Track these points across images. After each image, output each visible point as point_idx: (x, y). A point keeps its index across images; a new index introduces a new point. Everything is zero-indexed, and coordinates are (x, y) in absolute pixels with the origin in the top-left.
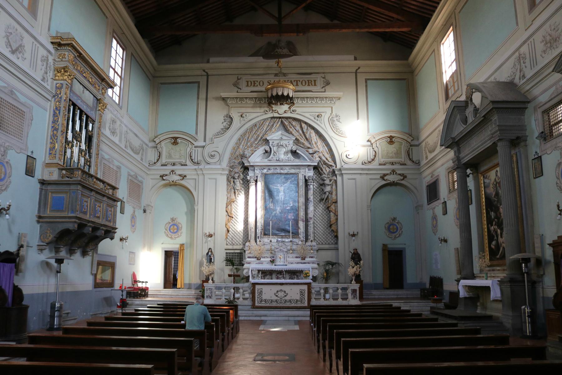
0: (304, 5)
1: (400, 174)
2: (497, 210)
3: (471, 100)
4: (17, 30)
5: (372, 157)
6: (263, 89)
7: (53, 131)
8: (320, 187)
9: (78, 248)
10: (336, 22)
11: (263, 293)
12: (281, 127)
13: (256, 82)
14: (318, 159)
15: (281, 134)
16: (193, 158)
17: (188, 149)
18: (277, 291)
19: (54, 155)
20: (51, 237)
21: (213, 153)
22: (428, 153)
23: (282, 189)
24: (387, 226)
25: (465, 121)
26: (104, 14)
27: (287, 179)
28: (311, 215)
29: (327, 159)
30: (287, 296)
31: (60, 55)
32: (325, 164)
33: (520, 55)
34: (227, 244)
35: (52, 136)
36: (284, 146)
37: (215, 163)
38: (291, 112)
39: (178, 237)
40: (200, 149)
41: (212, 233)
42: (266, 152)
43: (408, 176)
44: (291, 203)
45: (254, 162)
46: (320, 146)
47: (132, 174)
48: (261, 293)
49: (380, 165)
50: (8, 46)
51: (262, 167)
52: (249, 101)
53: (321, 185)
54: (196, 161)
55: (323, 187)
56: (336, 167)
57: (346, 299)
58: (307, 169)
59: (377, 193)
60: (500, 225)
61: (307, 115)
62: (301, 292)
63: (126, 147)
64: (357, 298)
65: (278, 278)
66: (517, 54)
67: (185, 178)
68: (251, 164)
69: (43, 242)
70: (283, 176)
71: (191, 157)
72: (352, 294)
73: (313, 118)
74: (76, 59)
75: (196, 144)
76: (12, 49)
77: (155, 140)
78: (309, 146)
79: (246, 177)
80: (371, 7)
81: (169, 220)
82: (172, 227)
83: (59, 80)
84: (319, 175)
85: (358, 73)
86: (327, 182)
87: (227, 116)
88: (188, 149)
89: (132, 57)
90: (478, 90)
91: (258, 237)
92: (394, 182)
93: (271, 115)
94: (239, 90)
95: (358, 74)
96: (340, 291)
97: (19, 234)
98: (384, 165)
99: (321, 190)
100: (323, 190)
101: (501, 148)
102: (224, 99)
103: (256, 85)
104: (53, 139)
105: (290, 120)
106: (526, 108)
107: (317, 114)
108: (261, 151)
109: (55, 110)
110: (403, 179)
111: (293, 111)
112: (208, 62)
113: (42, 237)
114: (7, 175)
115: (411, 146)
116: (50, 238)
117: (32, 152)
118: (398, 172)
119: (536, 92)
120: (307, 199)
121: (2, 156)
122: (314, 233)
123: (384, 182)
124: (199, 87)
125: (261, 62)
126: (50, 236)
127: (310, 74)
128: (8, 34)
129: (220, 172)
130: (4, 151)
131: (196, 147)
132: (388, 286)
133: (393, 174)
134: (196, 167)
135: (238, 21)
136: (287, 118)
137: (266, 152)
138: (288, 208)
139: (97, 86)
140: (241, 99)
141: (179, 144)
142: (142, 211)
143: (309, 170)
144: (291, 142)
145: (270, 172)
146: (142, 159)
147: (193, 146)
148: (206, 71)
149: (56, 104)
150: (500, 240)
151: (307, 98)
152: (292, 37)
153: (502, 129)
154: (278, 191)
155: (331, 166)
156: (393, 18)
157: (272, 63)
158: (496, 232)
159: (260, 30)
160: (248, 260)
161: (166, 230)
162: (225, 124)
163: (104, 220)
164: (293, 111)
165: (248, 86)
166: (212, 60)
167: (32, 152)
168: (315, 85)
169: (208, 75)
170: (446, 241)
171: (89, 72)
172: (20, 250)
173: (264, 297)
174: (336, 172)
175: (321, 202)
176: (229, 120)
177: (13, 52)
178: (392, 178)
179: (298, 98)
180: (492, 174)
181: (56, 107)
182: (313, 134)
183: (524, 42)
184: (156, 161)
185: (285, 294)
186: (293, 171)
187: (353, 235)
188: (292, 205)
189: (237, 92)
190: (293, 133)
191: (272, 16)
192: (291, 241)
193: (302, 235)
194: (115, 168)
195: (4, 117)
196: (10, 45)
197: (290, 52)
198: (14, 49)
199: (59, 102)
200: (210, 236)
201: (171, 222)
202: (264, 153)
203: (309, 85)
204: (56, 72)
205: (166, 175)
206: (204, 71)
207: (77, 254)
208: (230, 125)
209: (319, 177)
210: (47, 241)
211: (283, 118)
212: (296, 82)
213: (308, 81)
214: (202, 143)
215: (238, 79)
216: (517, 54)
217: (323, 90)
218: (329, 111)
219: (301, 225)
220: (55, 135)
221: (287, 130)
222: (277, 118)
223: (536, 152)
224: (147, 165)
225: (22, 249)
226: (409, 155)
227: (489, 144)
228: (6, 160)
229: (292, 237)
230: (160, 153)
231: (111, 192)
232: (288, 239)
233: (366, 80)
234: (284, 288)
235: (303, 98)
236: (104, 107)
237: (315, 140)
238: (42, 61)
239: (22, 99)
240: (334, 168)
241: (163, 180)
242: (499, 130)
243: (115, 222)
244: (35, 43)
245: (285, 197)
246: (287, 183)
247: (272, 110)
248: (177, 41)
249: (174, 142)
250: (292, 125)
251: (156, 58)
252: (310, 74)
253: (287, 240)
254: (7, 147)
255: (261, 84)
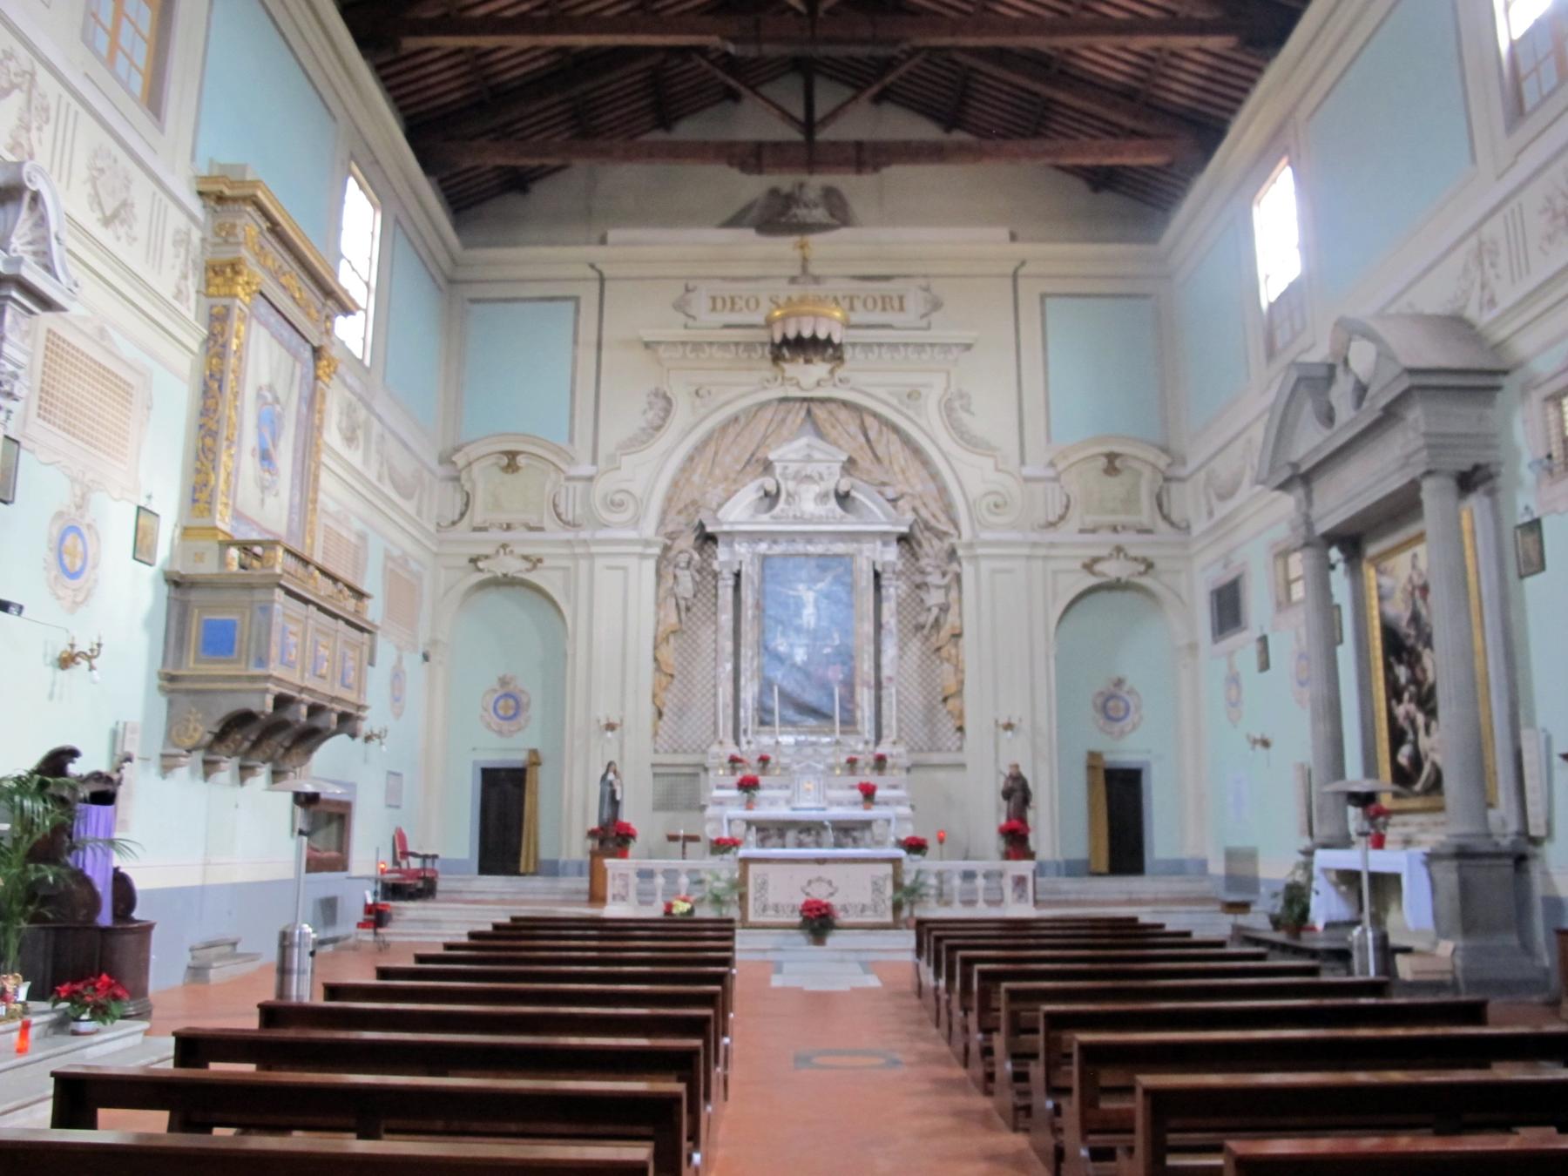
0: (875, 89)
1: (1135, 559)
2: (1413, 660)
3: (1346, 362)
4: (115, 161)
5: (1059, 511)
6: (759, 319)
7: (203, 438)
8: (913, 591)
9: (229, 757)
10: (959, 136)
11: (770, 888)
12: (808, 426)
13: (737, 300)
14: (910, 517)
15: (809, 446)
16: (562, 509)
17: (548, 487)
18: (810, 882)
19: (207, 506)
20: (202, 731)
21: (618, 497)
22: (1214, 501)
23: (809, 597)
24: (1099, 701)
25: (1328, 417)
26: (328, 108)
27: (823, 569)
28: (887, 671)
29: (934, 516)
30: (837, 895)
31: (221, 227)
32: (928, 527)
33: (1481, 244)
34: (656, 751)
35: (201, 453)
36: (817, 478)
37: (624, 525)
38: (835, 385)
39: (519, 730)
40: (580, 486)
41: (615, 719)
42: (767, 494)
43: (1160, 565)
44: (836, 636)
45: (732, 523)
46: (918, 483)
47: (396, 553)
48: (763, 886)
49: (1082, 531)
50: (95, 206)
51: (754, 537)
52: (717, 353)
53: (918, 587)
54: (570, 518)
55: (923, 594)
56: (960, 536)
57: (998, 902)
58: (879, 544)
59: (1078, 606)
60: (1427, 701)
61: (881, 393)
62: (875, 883)
63: (380, 478)
64: (1027, 901)
65: (800, 845)
66: (1472, 242)
67: (539, 565)
68: (726, 528)
69: (176, 746)
70: (813, 563)
71: (555, 506)
72: (1014, 890)
73: (895, 402)
74: (265, 237)
75: (574, 472)
76: (103, 213)
77: (454, 459)
78: (886, 479)
79: (710, 565)
80: (1061, 96)
81: (495, 684)
82: (501, 703)
83: (220, 296)
84: (913, 560)
85: (1026, 276)
86: (934, 579)
87: (656, 394)
88: (548, 487)
89: (399, 230)
90: (1369, 335)
91: (745, 731)
92: (1118, 580)
93: (781, 393)
94: (690, 322)
95: (1021, 282)
96: (980, 882)
97: (117, 723)
98: (1093, 531)
99: (918, 600)
100: (922, 601)
101: (1434, 496)
102: (647, 345)
103: (737, 307)
104: (204, 460)
105: (833, 406)
106: (1498, 388)
107: (908, 390)
108: (749, 494)
109: (208, 379)
110: (1145, 573)
111: (841, 381)
112: (603, 241)
113: (174, 733)
114: (90, 562)
115: (1167, 479)
116: (197, 736)
117: (149, 497)
118: (1133, 552)
119: (1524, 346)
120: (878, 626)
121: (79, 507)
122: (899, 720)
123: (1092, 581)
124: (577, 311)
125: (749, 242)
126: (195, 730)
127: (887, 278)
128: (95, 173)
129: (639, 549)
130: (83, 497)
131: (569, 479)
132: (1103, 865)
133: (1118, 557)
134: (569, 535)
135: (688, 130)
136: (823, 401)
137: (767, 494)
138: (827, 650)
139: (313, 311)
140: (697, 346)
141: (521, 472)
142: (419, 657)
143: (885, 544)
144: (837, 467)
145: (778, 549)
146: (419, 513)
147: (562, 476)
148: (599, 266)
149: (211, 363)
150: (1424, 742)
151: (880, 345)
152: (847, 182)
153: (1436, 444)
154: (799, 605)
155: (946, 534)
156: (1036, 94)
157: (784, 246)
158: (1413, 722)
159: (753, 157)
160: (717, 793)
161: (486, 710)
162: (650, 415)
163: (337, 685)
164: (841, 381)
165: (714, 309)
166: (613, 235)
167: (149, 497)
168: (902, 309)
169: (602, 280)
170: (1266, 744)
171: (294, 274)
172: (123, 768)
173: (772, 897)
174: (960, 552)
175: (919, 635)
176: (661, 403)
177: (107, 222)
178: (1113, 569)
179: (854, 345)
180: (1401, 565)
181: (211, 370)
182: (896, 446)
183: (1493, 211)
184: (456, 517)
185: (831, 890)
186: (840, 548)
187: (1009, 726)
188: (837, 642)
189: (686, 327)
190: (841, 442)
191: (790, 118)
192: (838, 743)
193: (866, 726)
194: (353, 539)
195: (55, 393)
196: (100, 204)
197: (832, 215)
198: (108, 213)
199: (220, 358)
200: (610, 727)
201: (497, 687)
202: (761, 498)
203: (884, 309)
204: (211, 274)
205: (487, 557)
206: (592, 266)
207: (259, 778)
208: (664, 419)
209: (913, 565)
210: (188, 743)
211: (811, 400)
212: (847, 300)
213: (883, 298)
214: (586, 469)
215: (687, 290)
216: (1472, 242)
217: (924, 323)
218: (939, 381)
219: (865, 697)
220: (210, 450)
221: (820, 433)
222: (795, 399)
223: (1527, 508)
224: (432, 528)
225: (127, 765)
226: (1160, 506)
227: (1396, 483)
228: (87, 520)
229: (842, 732)
230: (468, 494)
231: (351, 604)
232: (826, 734)
233: (1043, 297)
234: (827, 871)
235: (868, 346)
236: (332, 369)
237: (903, 462)
238: (176, 243)
239: (127, 350)
240: (954, 540)
241: (480, 570)
242: (1429, 446)
243: (360, 690)
244: (160, 194)
245: (819, 618)
246: (823, 581)
247: (783, 378)
248: (518, 182)
249: (509, 465)
250: (837, 420)
251: (457, 226)
252: (887, 278)
253: (826, 740)
254: (90, 484)
255: (752, 304)
